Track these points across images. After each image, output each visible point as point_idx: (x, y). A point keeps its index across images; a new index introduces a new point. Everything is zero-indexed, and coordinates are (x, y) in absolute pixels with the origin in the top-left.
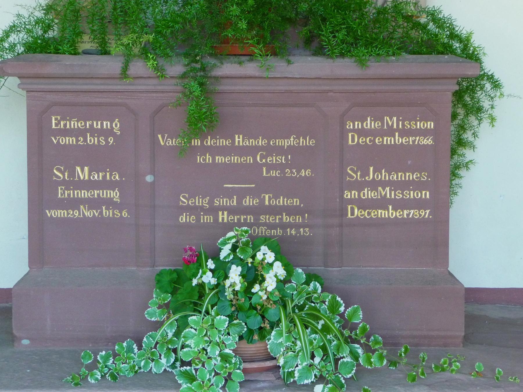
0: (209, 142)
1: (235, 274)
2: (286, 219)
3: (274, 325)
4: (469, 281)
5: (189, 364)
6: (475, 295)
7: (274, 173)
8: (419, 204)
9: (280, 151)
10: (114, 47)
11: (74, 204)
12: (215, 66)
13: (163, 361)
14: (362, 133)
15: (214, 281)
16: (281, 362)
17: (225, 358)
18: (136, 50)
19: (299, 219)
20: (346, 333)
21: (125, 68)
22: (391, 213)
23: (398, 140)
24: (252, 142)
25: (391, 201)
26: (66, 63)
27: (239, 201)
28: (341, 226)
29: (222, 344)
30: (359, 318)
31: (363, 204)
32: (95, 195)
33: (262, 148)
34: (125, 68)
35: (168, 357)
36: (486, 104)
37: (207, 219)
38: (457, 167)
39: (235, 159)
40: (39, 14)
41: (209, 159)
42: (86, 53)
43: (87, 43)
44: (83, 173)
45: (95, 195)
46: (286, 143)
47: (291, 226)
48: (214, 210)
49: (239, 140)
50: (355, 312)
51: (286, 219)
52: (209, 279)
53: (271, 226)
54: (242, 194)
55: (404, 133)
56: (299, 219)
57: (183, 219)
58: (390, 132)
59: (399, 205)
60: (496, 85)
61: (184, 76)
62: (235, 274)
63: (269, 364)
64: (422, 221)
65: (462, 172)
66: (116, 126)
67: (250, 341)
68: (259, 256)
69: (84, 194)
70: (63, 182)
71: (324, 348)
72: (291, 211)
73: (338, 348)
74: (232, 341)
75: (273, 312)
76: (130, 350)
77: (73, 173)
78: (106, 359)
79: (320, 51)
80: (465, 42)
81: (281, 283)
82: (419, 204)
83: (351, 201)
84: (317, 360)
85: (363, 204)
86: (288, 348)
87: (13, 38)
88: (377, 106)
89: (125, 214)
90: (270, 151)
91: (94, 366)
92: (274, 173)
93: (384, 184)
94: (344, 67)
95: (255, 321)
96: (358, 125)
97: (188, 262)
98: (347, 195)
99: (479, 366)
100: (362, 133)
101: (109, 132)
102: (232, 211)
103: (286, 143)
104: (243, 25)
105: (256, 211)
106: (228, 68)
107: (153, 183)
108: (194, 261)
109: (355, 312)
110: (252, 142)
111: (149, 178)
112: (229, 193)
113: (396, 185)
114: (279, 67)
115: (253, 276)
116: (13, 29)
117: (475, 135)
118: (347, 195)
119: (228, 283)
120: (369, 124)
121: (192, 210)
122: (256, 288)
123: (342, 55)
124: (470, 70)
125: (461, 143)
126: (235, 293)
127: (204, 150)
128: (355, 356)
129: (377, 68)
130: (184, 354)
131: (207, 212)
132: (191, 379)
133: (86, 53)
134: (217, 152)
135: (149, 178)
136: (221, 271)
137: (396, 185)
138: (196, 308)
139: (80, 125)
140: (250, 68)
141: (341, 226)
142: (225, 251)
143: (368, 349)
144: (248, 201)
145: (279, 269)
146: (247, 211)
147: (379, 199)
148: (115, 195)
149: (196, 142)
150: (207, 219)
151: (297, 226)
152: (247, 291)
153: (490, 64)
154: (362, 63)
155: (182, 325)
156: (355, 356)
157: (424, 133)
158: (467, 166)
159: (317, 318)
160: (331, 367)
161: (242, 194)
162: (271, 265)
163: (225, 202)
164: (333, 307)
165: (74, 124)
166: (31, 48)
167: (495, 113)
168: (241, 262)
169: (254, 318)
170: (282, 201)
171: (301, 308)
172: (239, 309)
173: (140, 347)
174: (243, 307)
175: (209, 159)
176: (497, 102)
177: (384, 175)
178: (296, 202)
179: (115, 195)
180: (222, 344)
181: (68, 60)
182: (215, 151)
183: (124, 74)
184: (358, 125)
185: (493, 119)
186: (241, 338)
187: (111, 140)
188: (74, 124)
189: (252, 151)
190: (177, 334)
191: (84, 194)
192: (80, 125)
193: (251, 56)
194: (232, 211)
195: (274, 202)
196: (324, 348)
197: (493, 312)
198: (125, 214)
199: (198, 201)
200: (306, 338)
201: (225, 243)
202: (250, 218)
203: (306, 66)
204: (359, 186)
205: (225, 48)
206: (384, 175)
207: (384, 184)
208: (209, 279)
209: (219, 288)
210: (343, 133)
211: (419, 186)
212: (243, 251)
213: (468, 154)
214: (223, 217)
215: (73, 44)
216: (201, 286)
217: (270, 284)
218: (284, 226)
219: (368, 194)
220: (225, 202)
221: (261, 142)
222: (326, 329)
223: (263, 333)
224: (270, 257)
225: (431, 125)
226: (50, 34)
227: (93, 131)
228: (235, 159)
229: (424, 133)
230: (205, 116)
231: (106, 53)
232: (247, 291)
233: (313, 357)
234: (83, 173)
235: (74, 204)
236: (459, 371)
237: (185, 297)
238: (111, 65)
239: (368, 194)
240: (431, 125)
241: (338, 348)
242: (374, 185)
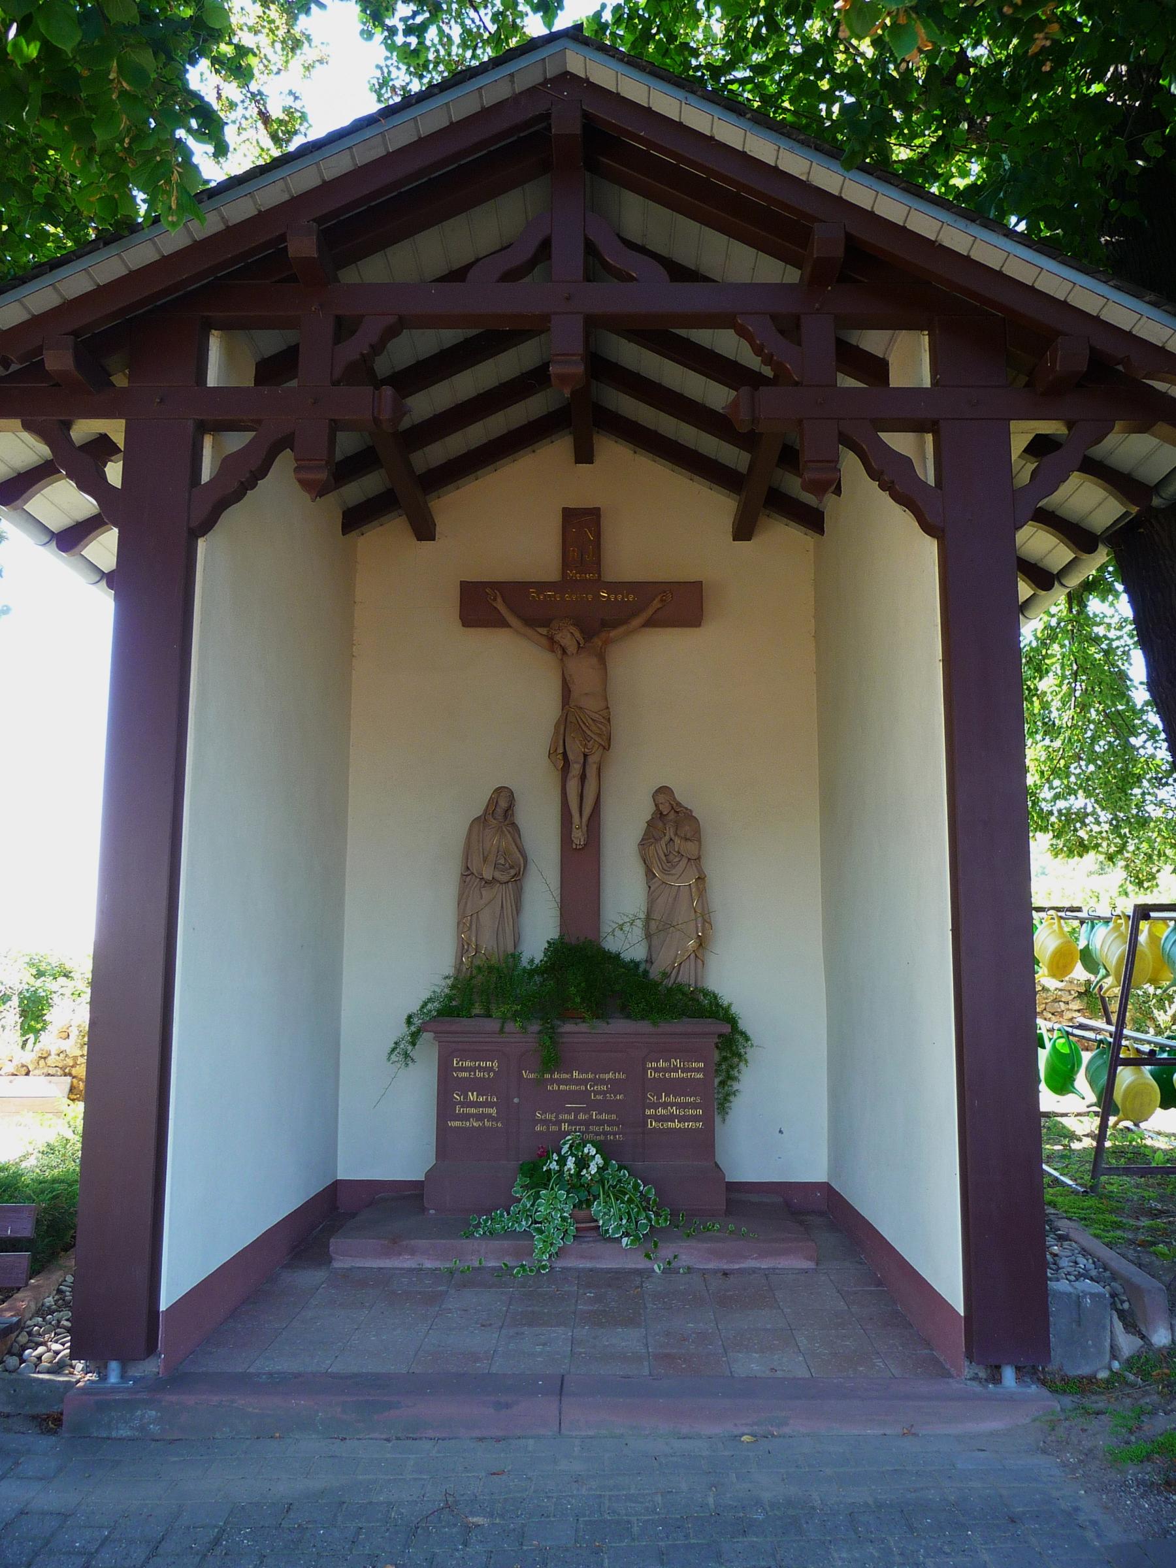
0: (556, 1076)
1: (571, 1163)
2: (607, 1128)
3: (596, 1197)
4: (732, 1177)
5: (540, 1223)
6: (733, 1187)
7: (600, 1097)
8: (695, 1118)
9: (602, 1082)
10: (496, 1013)
11: (467, 1117)
12: (559, 1026)
13: (524, 1223)
14: (657, 1070)
15: (557, 1168)
16: (601, 1222)
17: (564, 1219)
18: (509, 1015)
19: (615, 1129)
20: (644, 1204)
21: (503, 1027)
22: (676, 1125)
23: (680, 1075)
24: (584, 1076)
25: (677, 1116)
26: (465, 1024)
27: (576, 1117)
28: (643, 1133)
29: (562, 1210)
30: (652, 1196)
31: (659, 1119)
32: (480, 1111)
33: (591, 1080)
34: (503, 1027)
35: (527, 1220)
36: (742, 1051)
37: (553, 1128)
38: (728, 1095)
39: (573, 1088)
40: (447, 991)
41: (556, 1087)
42: (477, 1016)
43: (477, 1010)
44: (472, 1097)
45: (480, 1111)
46: (607, 1077)
47: (610, 1133)
48: (558, 1123)
49: (575, 1074)
50: (650, 1189)
51: (607, 1128)
52: (554, 1166)
53: (597, 1134)
54: (577, 1111)
55: (684, 1070)
56: (615, 1129)
57: (538, 1128)
58: (675, 1070)
59: (682, 1119)
60: (747, 1039)
61: (540, 1032)
62: (571, 1163)
63: (593, 1224)
64: (697, 1130)
65: (732, 1098)
66: (495, 1064)
67: (580, 1208)
68: (586, 1151)
69: (473, 1111)
70: (460, 1103)
71: (629, 1213)
72: (610, 1123)
73: (638, 1213)
74: (568, 1208)
75: (595, 1189)
76: (502, 1216)
77: (466, 1096)
78: (486, 1221)
79: (628, 1017)
80: (727, 1010)
81: (601, 1170)
82: (695, 1118)
83: (650, 1116)
84: (624, 1222)
85: (659, 1119)
86: (605, 1214)
87: (430, 1006)
88: (667, 1052)
89: (500, 1125)
90: (597, 1082)
91: (478, 1225)
92: (600, 1097)
93: (672, 1105)
94: (644, 1027)
95: (584, 1195)
96: (654, 1065)
97: (540, 1156)
98: (648, 1112)
99: (731, 1227)
100: (657, 1070)
101: (491, 1069)
102: (570, 1123)
103: (607, 1077)
104: (578, 1000)
105: (589, 1123)
106: (569, 1027)
107: (991, 115)
108: (545, 1156)
109: (650, 1189)
110: (584, 1076)
111: (516, 1100)
112: (569, 1111)
113: (680, 1106)
114: (601, 1027)
115: (583, 1163)
116: (430, 1000)
117: (739, 1072)
118: (648, 1112)
119: (566, 1169)
120: (662, 1064)
121: (544, 1122)
122: (584, 1172)
123: (643, 1019)
124: (726, 1029)
125: (730, 1077)
126: (570, 1175)
127: (552, 1081)
128: (649, 1219)
129: (665, 1027)
130: (538, 1216)
131: (555, 1124)
132: (541, 1232)
133: (477, 1016)
134: (561, 1082)
135: (516, 1100)
136: (562, 1161)
137: (680, 1106)
138: (545, 1187)
139: (472, 1064)
140: (583, 1027)
141: (643, 1133)
142: (565, 1149)
143: (657, 1215)
144: (581, 1117)
145: (599, 1159)
146: (580, 1123)
147: (671, 1115)
148: (493, 1111)
149: (547, 1076)
150: (553, 1128)
151: (615, 1134)
152: (578, 1174)
153: (743, 1025)
154: (654, 1024)
155: (537, 1196)
156: (649, 1219)
157: (698, 1070)
158: (734, 1094)
159: (625, 1194)
160: (633, 1226)
161: (577, 1111)
162: (594, 1157)
163: (566, 1117)
164: (636, 1186)
165: (468, 1064)
166: (441, 1013)
167: (747, 1056)
168: (572, 1155)
169: (583, 1192)
170: (604, 1116)
171: (614, 1187)
172: (573, 1187)
173: (508, 1214)
174: (575, 1185)
175: (556, 1087)
176: (748, 1050)
177: (671, 1099)
178: (614, 1117)
179: (493, 1111)
180: (562, 1210)
181: (465, 1021)
182: (560, 1082)
183: (502, 1031)
184: (654, 1065)
185: (746, 1061)
186: (574, 1206)
187: (492, 1075)
188: (468, 1064)
189: (584, 1082)
190: (532, 1205)
191: (473, 1111)
192: (472, 1064)
193: (583, 1020)
194: (570, 1123)
195: (599, 1117)
196: (629, 1213)
197: (754, 1198)
198: (500, 1125)
199: (548, 1116)
200: (617, 1207)
201: (565, 1144)
202: (583, 1128)
203: (620, 1026)
204: (655, 1106)
205: (568, 1015)
206: (671, 1099)
207: (672, 1105)
208: (554, 1166)
209: (561, 1172)
210: (645, 1070)
211: (694, 1106)
212: (577, 1149)
213: (736, 1086)
214: (565, 1127)
215: (469, 1012)
216: (549, 1171)
217: (593, 1169)
218: (605, 1133)
219: (661, 1111)
220: (566, 1117)
221: (590, 1076)
222: (630, 1201)
223: (589, 1204)
224: (593, 1151)
225: (702, 1065)
226: (454, 1003)
227: (480, 1068)
228: (573, 1088)
229: (698, 1070)
230: (554, 1057)
231: (490, 1016)
232: (578, 1174)
233: (621, 1219)
234: (472, 1097)
235: (467, 1117)
236: (719, 1230)
237: (538, 1179)
238: (493, 1025)
239: (661, 1111)
240: (702, 1065)
241: (638, 1213)
242: (665, 1105)
